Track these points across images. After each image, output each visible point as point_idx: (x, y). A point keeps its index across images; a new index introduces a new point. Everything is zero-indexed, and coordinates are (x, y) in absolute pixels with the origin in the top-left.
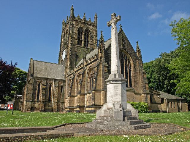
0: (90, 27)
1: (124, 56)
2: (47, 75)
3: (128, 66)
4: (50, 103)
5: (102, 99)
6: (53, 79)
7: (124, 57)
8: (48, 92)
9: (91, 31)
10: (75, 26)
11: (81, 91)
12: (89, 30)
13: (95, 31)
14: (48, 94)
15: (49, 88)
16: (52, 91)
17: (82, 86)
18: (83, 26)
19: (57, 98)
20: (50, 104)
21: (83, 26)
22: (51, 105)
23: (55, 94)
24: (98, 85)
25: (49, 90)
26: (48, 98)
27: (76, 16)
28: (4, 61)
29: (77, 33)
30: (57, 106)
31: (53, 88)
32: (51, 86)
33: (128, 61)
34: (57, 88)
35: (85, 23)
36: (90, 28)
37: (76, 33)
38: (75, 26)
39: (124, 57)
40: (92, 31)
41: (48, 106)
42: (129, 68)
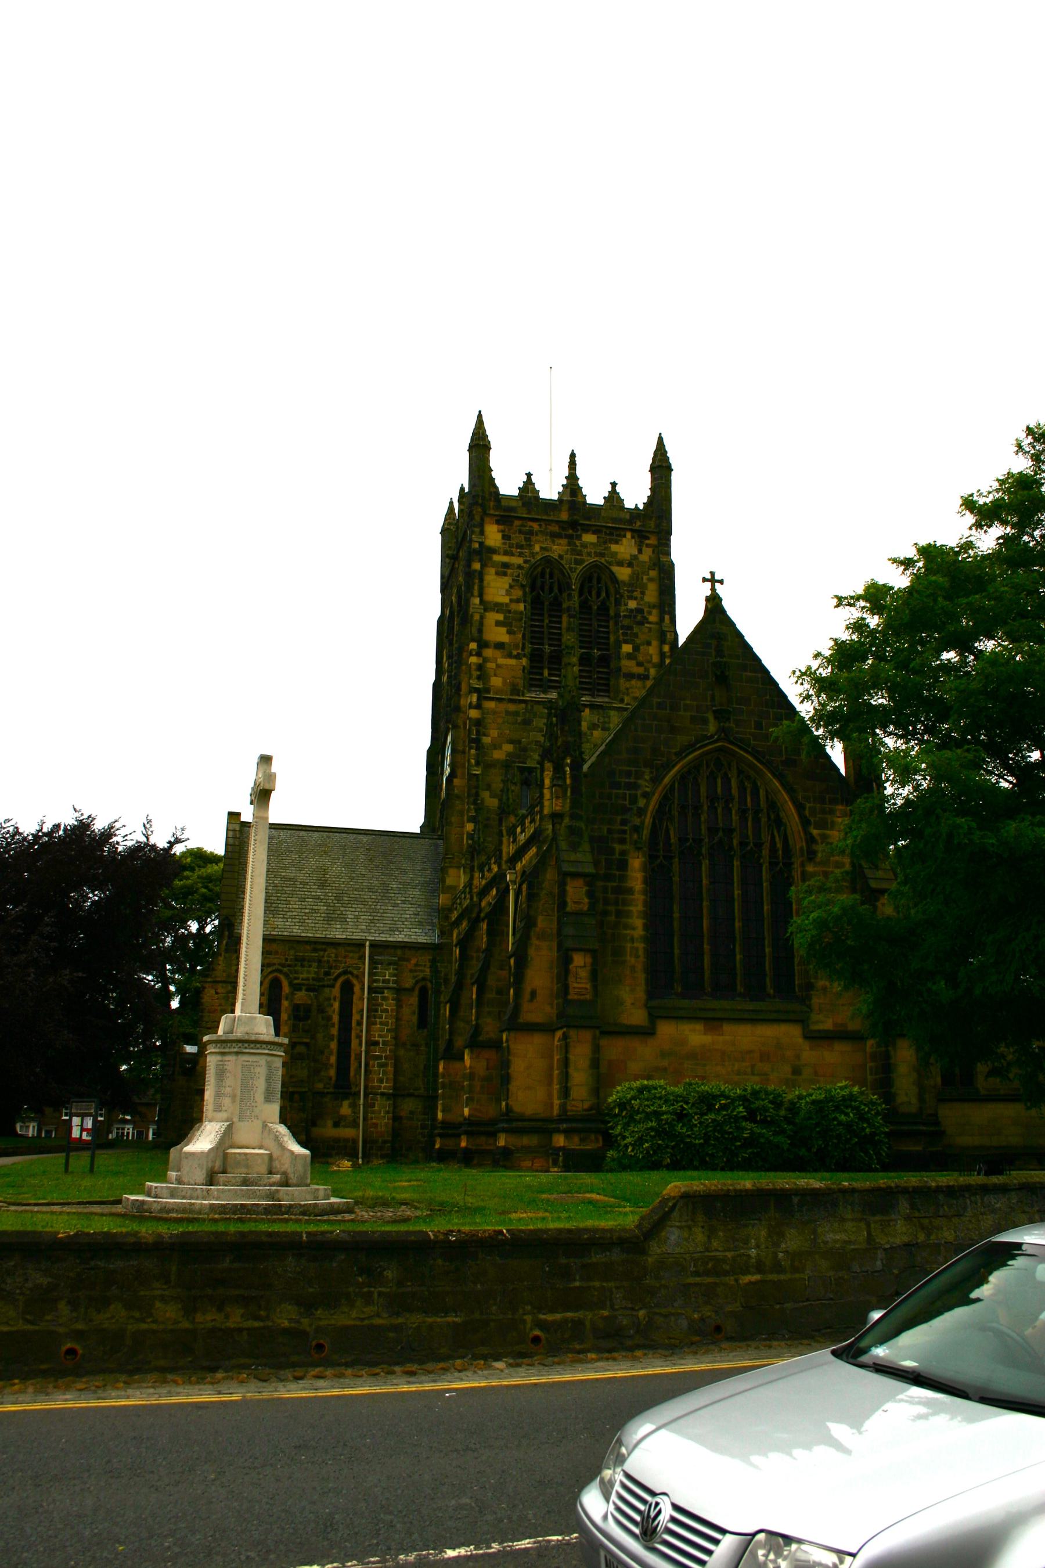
0: (614, 548)
1: (734, 783)
2: (329, 919)
3: (765, 852)
4: (346, 1103)
5: (555, 1081)
6: (360, 945)
7: (735, 792)
8: (335, 1031)
9: (623, 573)
10: (505, 559)
11: (477, 1030)
12: (612, 575)
13: (653, 574)
14: (334, 1045)
15: (336, 1005)
16: (360, 1023)
17: (490, 995)
18: (558, 549)
19: (390, 1068)
20: (345, 1109)
21: (558, 549)
22: (356, 1112)
23: (377, 1043)
24: (533, 994)
25: (336, 1018)
26: (332, 1072)
27: (508, 485)
28: (99, 825)
29: (521, 607)
30: (396, 1118)
31: (362, 1003)
32: (347, 989)
33: (764, 820)
34: (388, 1004)
35: (573, 525)
36: (614, 554)
37: (514, 607)
38: (505, 559)
39: (735, 792)
40: (636, 577)
41: (336, 1125)
42: (772, 865)
